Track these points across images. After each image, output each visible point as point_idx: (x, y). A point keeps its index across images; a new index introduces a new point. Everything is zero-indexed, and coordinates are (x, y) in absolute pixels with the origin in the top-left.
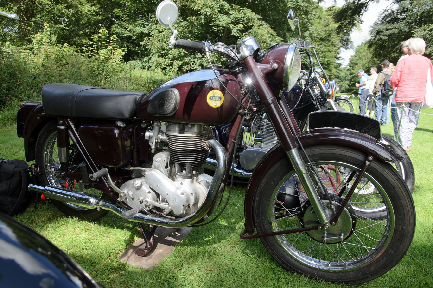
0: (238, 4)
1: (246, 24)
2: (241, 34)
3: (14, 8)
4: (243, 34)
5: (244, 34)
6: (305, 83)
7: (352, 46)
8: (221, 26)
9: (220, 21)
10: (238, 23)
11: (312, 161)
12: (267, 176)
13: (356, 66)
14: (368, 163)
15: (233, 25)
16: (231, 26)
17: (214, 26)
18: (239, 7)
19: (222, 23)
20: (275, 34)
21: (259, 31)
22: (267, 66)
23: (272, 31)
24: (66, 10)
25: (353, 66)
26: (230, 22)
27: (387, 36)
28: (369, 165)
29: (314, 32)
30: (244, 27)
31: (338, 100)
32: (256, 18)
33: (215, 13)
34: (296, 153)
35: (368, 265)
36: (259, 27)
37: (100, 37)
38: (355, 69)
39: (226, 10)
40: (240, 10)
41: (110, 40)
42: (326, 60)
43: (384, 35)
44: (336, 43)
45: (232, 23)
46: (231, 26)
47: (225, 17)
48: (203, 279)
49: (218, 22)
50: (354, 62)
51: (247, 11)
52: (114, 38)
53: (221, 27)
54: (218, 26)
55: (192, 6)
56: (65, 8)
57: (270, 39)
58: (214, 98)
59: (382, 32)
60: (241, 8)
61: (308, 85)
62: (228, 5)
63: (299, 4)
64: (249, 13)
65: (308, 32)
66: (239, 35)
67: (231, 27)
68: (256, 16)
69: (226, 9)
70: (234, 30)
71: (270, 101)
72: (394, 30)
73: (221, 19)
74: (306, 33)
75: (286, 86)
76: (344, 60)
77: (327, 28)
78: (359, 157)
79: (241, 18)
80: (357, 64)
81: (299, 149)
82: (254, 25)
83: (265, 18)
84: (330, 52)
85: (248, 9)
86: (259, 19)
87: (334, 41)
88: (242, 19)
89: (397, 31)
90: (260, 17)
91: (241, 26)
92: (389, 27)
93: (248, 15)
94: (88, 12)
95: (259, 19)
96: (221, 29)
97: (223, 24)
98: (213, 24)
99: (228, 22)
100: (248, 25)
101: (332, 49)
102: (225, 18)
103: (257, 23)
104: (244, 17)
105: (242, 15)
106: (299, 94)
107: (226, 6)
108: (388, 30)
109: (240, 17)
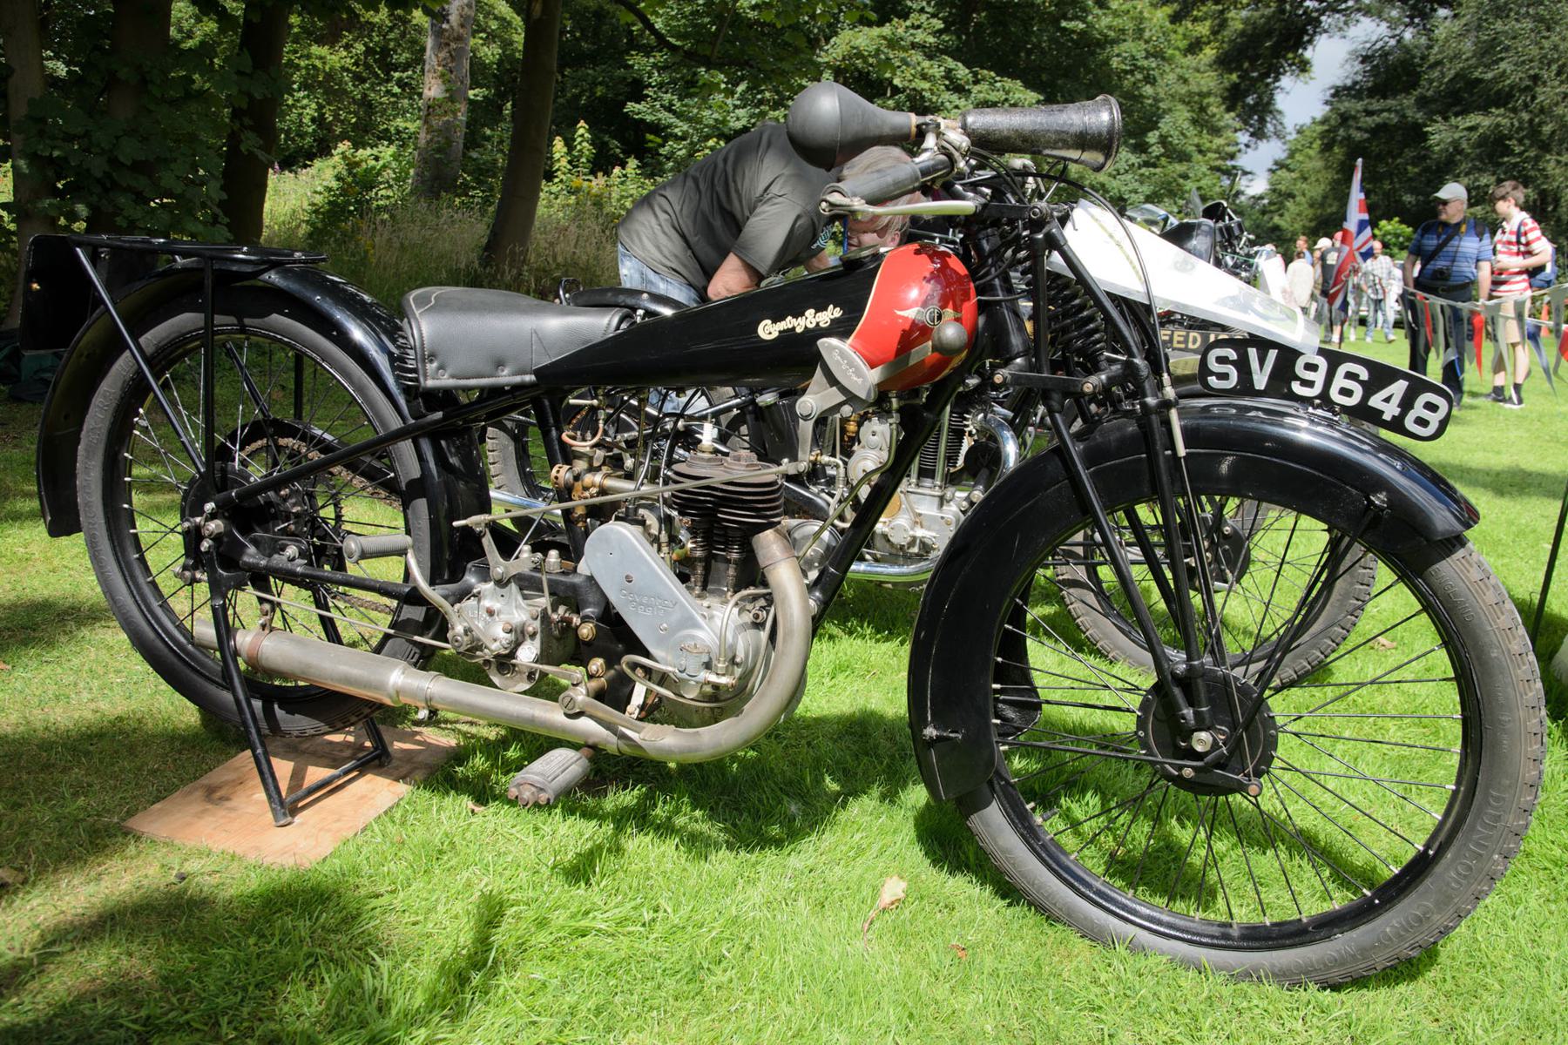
0: (990, 69)
3: (356, 45)
7: (1279, 127)
13: (1289, 204)
18: (993, 74)
25: (1282, 203)
27: (1366, 131)
38: (1286, 214)
43: (1359, 129)
50: (1282, 188)
59: (1355, 118)
60: (998, 78)
62: (967, 71)
63: (1139, 64)
65: (1157, 133)
72: (1385, 114)
74: (1150, 134)
76: (1250, 176)
80: (1291, 196)
89: (1394, 118)
90: (1042, 98)
92: (1376, 105)
101: (1208, 145)
102: (957, 102)
108: (1369, 113)
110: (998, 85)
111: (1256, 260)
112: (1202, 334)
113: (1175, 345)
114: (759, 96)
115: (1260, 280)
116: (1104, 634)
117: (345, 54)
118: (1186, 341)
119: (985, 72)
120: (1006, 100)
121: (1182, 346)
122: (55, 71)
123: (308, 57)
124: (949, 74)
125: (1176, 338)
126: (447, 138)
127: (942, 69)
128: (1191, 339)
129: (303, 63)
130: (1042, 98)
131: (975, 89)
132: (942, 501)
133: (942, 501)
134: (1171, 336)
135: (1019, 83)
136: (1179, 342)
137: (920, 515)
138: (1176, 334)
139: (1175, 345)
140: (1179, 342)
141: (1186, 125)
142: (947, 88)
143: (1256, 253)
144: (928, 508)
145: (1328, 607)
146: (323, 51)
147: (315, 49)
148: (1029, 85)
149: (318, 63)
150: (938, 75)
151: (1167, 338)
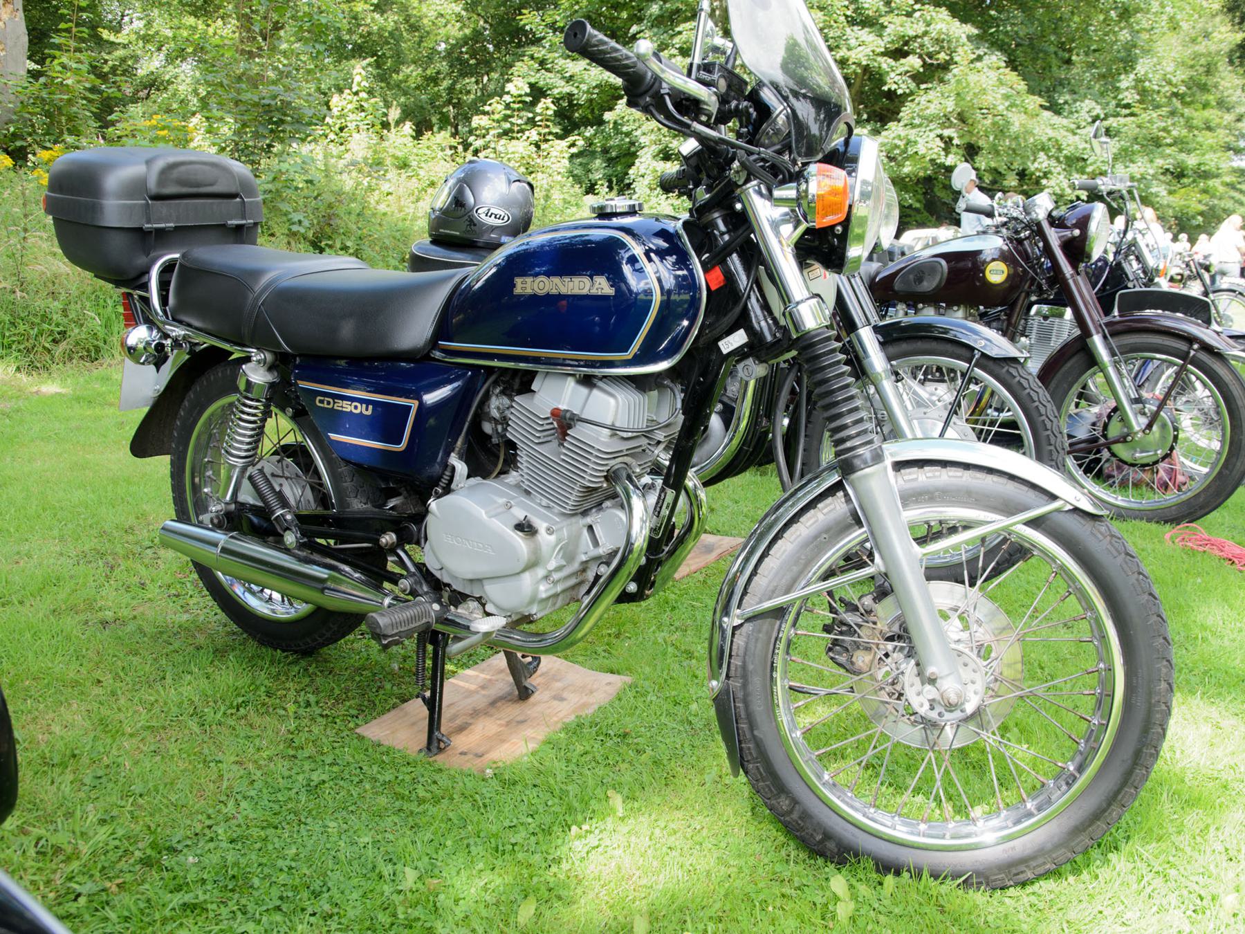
1: (930, 56)
2: (913, 85)
4: (919, 89)
5: (923, 86)
6: (1114, 249)
8: (854, 63)
9: (849, 49)
10: (905, 55)
11: (1121, 354)
12: (1059, 375)
14: (1192, 353)
15: (890, 61)
16: (886, 63)
21: (973, 78)
22: (1068, 233)
24: (377, 16)
26: (883, 50)
28: (1194, 356)
29: (1150, 76)
30: (925, 65)
31: (1214, 292)
32: (964, 36)
33: (835, 25)
36: (972, 66)
37: (508, 106)
40: (914, 11)
41: (536, 114)
42: (630, 806)
44: (1234, 99)
45: (888, 53)
47: (865, 34)
49: (844, 49)
51: (934, 14)
52: (547, 108)
53: (854, 66)
56: (373, 11)
57: (1007, 104)
58: (996, 272)
61: (1120, 253)
66: (907, 91)
67: (884, 66)
68: (961, 31)
69: (868, 9)
70: (892, 75)
71: (1068, 276)
73: (853, 42)
75: (1089, 257)
77: (1201, 48)
78: (1183, 346)
79: (917, 37)
81: (1105, 337)
82: (956, 59)
83: (989, 38)
84: (1209, 128)
85: (937, 9)
87: (1228, 89)
88: (919, 40)
91: (914, 62)
93: (938, 27)
94: (436, 18)
96: (854, 72)
97: (860, 56)
99: (873, 51)
100: (937, 59)
101: (1218, 120)
103: (964, 53)
104: (925, 33)
105: (921, 28)
106: (1102, 269)
109: (911, 33)
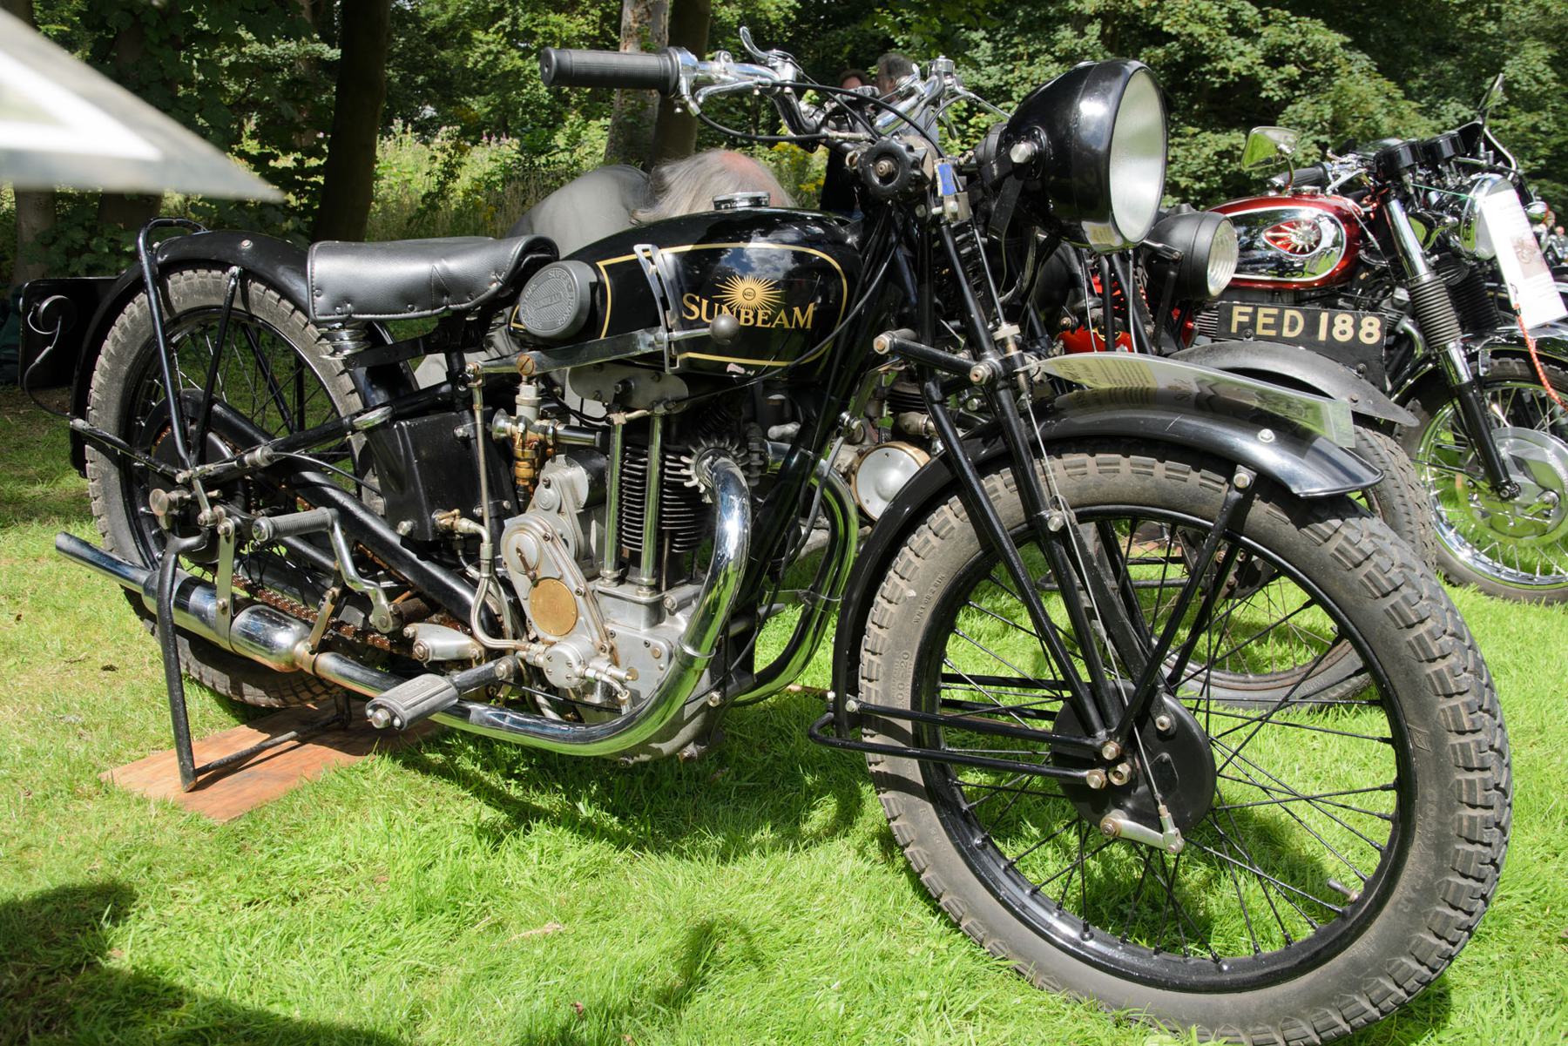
17: (1208, 72)
19: (1236, 65)
20: (1399, 94)
23: (1389, 86)
34: (1121, 420)
35: (184, 703)
39: (1249, 25)
46: (1262, 72)
48: (1552, 1005)
54: (1224, 72)
55: (1157, 20)
57: (1385, 111)
60: (1293, 19)
62: (1255, 10)
64: (1327, 38)
67: (1262, 75)
68: (1333, 39)
73: (1231, 53)
86: (1344, 45)
90: (1348, 40)
93: (1316, 37)
95: (1344, 45)
98: (1208, 67)
105: (1297, 38)
107: (1250, 13)
109: (1288, 42)
110: (1293, 26)
111: (1471, 195)
112: (1305, 314)
113: (1260, 331)
114: (1012, 51)
115: (1475, 228)
116: (950, 883)
117: (582, 20)
118: (1278, 325)
119: (1278, 11)
120: (1303, 43)
121: (1272, 333)
122: (321, 54)
123: (546, 24)
124: (1233, 16)
125: (1261, 320)
126: (643, 101)
127: (1225, 10)
128: (1287, 322)
129: (540, 30)
130: (1348, 40)
131: (1266, 31)
132: (657, 612)
133: (657, 612)
134: (1254, 317)
135: (1320, 22)
136: (1266, 326)
137: (613, 635)
138: (1261, 311)
139: (1260, 331)
140: (1266, 326)
141: (1541, 66)
142: (1230, 32)
143: (1473, 183)
144: (630, 625)
145: (1387, 909)
146: (561, 18)
147: (553, 17)
148: (1332, 25)
149: (556, 30)
150: (1219, 18)
151: (1245, 319)
